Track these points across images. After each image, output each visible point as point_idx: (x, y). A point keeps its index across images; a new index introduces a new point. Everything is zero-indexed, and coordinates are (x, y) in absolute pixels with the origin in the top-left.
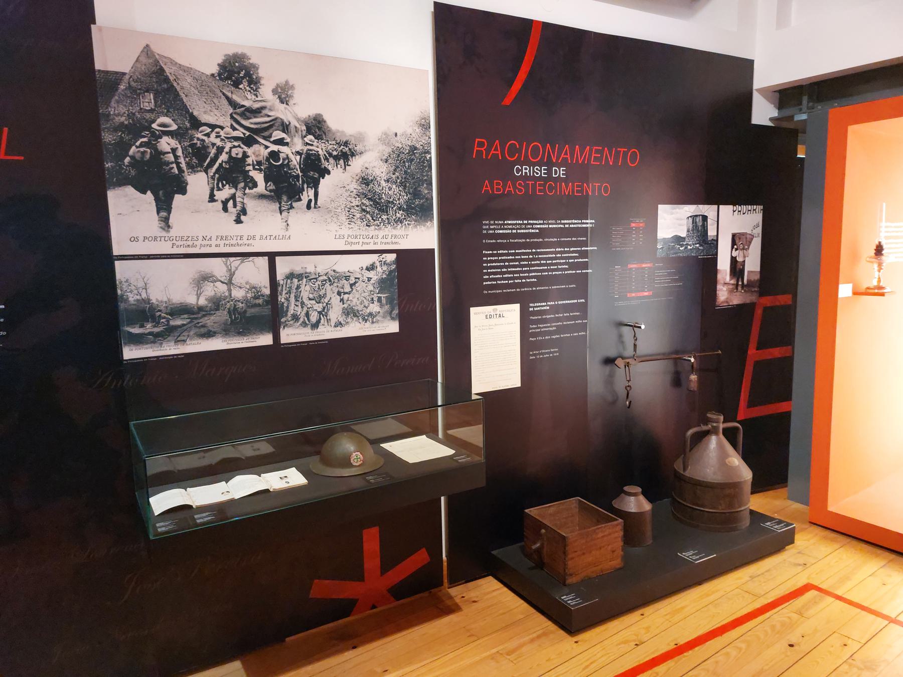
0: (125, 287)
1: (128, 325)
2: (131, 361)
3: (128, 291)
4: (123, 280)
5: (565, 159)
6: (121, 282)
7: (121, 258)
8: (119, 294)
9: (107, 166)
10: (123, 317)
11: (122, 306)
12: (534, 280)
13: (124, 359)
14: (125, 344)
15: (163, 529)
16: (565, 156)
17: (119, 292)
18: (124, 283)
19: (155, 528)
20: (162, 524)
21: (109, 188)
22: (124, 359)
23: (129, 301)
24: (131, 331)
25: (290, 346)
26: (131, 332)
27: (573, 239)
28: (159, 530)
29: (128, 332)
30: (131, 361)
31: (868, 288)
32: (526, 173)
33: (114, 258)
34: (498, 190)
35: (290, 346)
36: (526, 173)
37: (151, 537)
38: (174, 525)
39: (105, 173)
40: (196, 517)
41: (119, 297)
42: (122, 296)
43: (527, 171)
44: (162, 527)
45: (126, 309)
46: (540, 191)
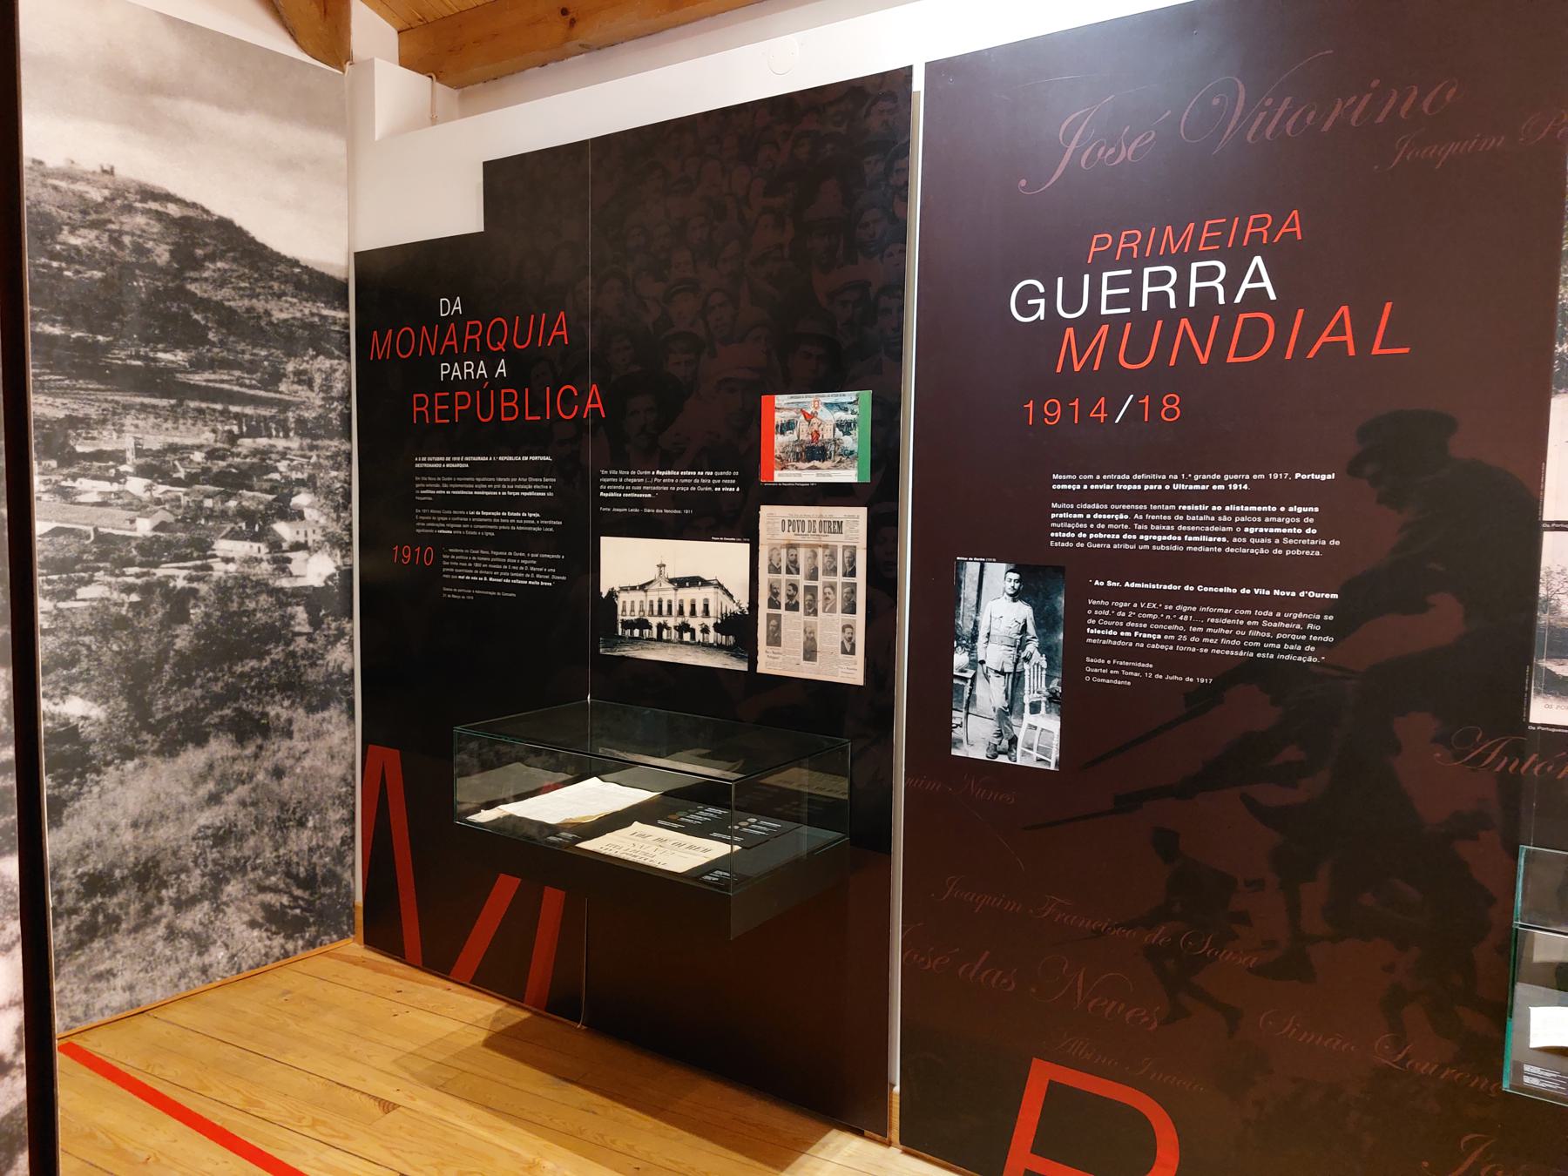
0: (1555, 584)
1: (1549, 658)
2: (1543, 729)
3: (1562, 591)
4: (1556, 569)
5: (450, 348)
6: (1549, 574)
7: (1558, 526)
8: (1541, 596)
9: (1560, 350)
10: (1542, 640)
11: (1544, 619)
12: (1094, 603)
13: (1531, 721)
14: (1538, 693)
15: (1535, 1082)
16: (558, 333)
17: (1543, 592)
18: (1557, 576)
19: (1518, 1071)
20: (1536, 1070)
21: (1557, 393)
22: (1531, 721)
23: (1560, 612)
24: (1553, 670)
25: (1554, 730)
26: (1554, 673)
27: (658, 511)
28: (1527, 1080)
29: (1548, 671)
30: (1543, 729)
31: (1007, 698)
32: (469, 374)
33: (1544, 525)
34: (510, 411)
35: (1554, 730)
36: (469, 374)
37: (1506, 1086)
38: (1562, 1085)
39: (1554, 364)
40: (1527, 1068)
41: (1540, 601)
42: (1548, 600)
43: (471, 370)
44: (1536, 1078)
45: (1551, 628)
46: (442, 414)
